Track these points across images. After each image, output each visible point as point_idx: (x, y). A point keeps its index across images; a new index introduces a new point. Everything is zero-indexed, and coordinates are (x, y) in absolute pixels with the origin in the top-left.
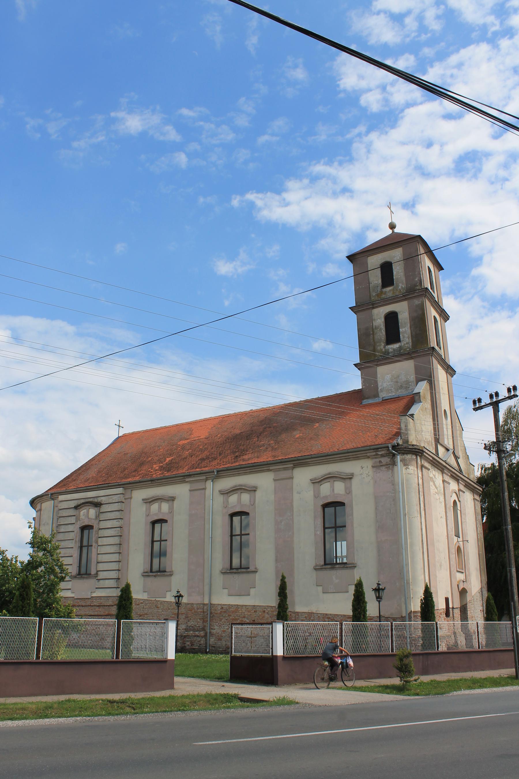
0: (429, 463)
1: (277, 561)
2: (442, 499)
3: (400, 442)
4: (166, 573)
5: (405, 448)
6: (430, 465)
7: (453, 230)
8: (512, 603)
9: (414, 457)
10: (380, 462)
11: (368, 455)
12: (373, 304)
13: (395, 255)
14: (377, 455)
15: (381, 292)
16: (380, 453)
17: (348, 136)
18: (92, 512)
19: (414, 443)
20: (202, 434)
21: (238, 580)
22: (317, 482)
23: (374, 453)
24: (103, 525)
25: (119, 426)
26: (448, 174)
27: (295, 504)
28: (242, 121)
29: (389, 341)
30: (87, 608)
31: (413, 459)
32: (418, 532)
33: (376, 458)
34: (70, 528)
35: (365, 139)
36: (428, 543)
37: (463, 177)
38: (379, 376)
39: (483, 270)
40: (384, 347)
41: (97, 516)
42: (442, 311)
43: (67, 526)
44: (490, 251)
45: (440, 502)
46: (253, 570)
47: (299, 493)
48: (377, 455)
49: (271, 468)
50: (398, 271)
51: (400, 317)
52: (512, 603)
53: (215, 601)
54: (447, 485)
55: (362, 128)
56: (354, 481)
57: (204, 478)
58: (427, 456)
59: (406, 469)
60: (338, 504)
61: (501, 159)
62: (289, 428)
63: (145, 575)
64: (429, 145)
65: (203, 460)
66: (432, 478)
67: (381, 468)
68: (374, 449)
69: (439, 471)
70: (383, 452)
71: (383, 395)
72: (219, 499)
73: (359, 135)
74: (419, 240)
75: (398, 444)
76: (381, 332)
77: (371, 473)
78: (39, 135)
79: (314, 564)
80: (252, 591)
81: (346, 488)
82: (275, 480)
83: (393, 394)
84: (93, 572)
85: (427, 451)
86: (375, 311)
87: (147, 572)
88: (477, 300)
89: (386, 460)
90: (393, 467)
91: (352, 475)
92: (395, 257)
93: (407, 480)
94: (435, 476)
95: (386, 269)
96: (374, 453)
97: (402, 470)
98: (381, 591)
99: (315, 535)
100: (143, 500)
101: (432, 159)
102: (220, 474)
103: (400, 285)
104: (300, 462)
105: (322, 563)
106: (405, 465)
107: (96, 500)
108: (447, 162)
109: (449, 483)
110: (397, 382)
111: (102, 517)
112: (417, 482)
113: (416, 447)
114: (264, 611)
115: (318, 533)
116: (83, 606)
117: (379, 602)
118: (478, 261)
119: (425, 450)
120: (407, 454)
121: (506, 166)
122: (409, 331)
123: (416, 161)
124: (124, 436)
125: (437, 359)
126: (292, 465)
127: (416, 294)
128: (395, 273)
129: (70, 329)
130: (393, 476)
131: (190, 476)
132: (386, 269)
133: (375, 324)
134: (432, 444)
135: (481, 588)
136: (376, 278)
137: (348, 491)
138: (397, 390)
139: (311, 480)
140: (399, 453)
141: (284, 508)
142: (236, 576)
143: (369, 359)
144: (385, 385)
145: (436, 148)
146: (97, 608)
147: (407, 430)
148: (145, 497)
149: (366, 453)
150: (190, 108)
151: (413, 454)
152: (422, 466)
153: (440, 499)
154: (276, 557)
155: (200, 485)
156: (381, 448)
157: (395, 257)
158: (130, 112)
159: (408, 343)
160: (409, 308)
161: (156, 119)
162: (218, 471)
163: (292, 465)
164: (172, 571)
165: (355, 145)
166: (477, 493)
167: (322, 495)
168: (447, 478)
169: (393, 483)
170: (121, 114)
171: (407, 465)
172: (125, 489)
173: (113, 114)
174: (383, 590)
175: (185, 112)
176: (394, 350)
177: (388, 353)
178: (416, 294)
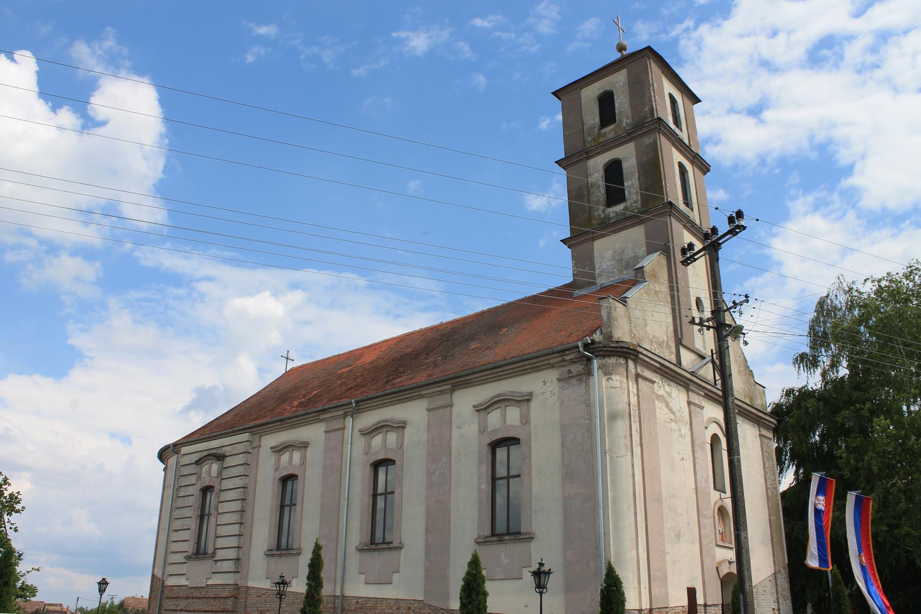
0: (655, 371)
1: (427, 531)
2: (686, 430)
3: (597, 337)
4: (292, 552)
5: (605, 347)
6: (659, 376)
7: (813, 136)
8: (741, 597)
9: (622, 361)
10: (569, 371)
11: (551, 361)
12: (587, 153)
13: (618, 81)
14: (564, 361)
15: (599, 135)
16: (568, 358)
17: (674, 33)
18: (215, 467)
19: (627, 339)
20: (368, 359)
21: (378, 560)
22: (483, 409)
23: (560, 359)
24: (227, 484)
25: (287, 358)
26: (802, 66)
27: (454, 444)
28: (545, 28)
29: (610, 202)
30: (201, 601)
31: (621, 365)
32: (626, 480)
33: (563, 366)
34: (191, 490)
35: (695, 35)
36: (650, 498)
37: (821, 68)
38: (596, 254)
39: (855, 181)
40: (604, 211)
41: (220, 473)
42: (694, 157)
43: (187, 488)
44: (863, 157)
45: (681, 436)
46: (396, 544)
47: (459, 427)
48: (564, 361)
49: (423, 393)
50: (622, 103)
51: (625, 165)
52: (741, 597)
53: (349, 593)
54: (697, 409)
55: (689, 23)
56: (534, 404)
57: (341, 412)
58: (648, 360)
59: (608, 380)
60: (510, 441)
61: (869, 40)
62: (472, 337)
63: (269, 554)
64: (775, 34)
65: (351, 388)
66: (662, 396)
67: (571, 381)
68: (558, 352)
69: (680, 388)
70: (572, 356)
71: (602, 281)
72: (360, 442)
73: (687, 30)
74: (650, 55)
75: (593, 342)
76: (600, 191)
77: (556, 391)
78: (314, 66)
79: (476, 536)
80: (396, 577)
81: (522, 416)
82: (428, 410)
83: (616, 278)
84: (210, 550)
85: (645, 352)
86: (591, 162)
87: (271, 550)
88: (851, 217)
89: (577, 368)
90: (588, 379)
91: (531, 394)
92: (617, 82)
93: (609, 398)
94: (669, 394)
95: (606, 101)
96: (560, 359)
97: (600, 382)
98: (543, 576)
99: (479, 489)
100: (271, 448)
101: (777, 50)
102: (359, 408)
103: (625, 120)
104: (460, 381)
105: (488, 533)
106: (606, 374)
107: (219, 452)
108: (799, 53)
109: (702, 408)
110: (621, 260)
111: (226, 473)
112: (626, 400)
113: (622, 344)
114: (409, 608)
115: (483, 486)
116: (197, 598)
117: (541, 593)
118: (849, 170)
119: (640, 350)
120: (609, 356)
121: (874, 50)
122: (637, 184)
123: (759, 55)
124: (292, 370)
125: (679, 220)
126: (449, 387)
127: (645, 130)
128: (617, 105)
129: (361, 282)
130: (588, 392)
131: (324, 411)
132: (606, 101)
133: (591, 180)
134: (668, 347)
135: (775, 574)
136: (592, 116)
137: (525, 420)
138: (621, 271)
139: (474, 407)
140: (597, 356)
141: (439, 451)
142: (375, 554)
143: (583, 231)
144: (604, 267)
145: (782, 37)
146: (212, 601)
147: (609, 318)
148: (274, 444)
149: (549, 359)
150: (483, 17)
151: (620, 356)
152: (638, 376)
153: (680, 430)
154: (427, 524)
155: (337, 424)
156: (568, 350)
157: (617, 82)
158: (415, 28)
159: (635, 202)
160: (637, 150)
161: (445, 34)
162: (357, 402)
163: (449, 387)
164: (300, 549)
165: (683, 43)
166: (767, 427)
167: (490, 429)
168: (695, 399)
169: (588, 404)
170: (402, 34)
171: (611, 374)
172: (253, 434)
173: (394, 35)
174: (549, 573)
175: (478, 22)
176: (617, 214)
177: (609, 219)
178: (645, 130)
